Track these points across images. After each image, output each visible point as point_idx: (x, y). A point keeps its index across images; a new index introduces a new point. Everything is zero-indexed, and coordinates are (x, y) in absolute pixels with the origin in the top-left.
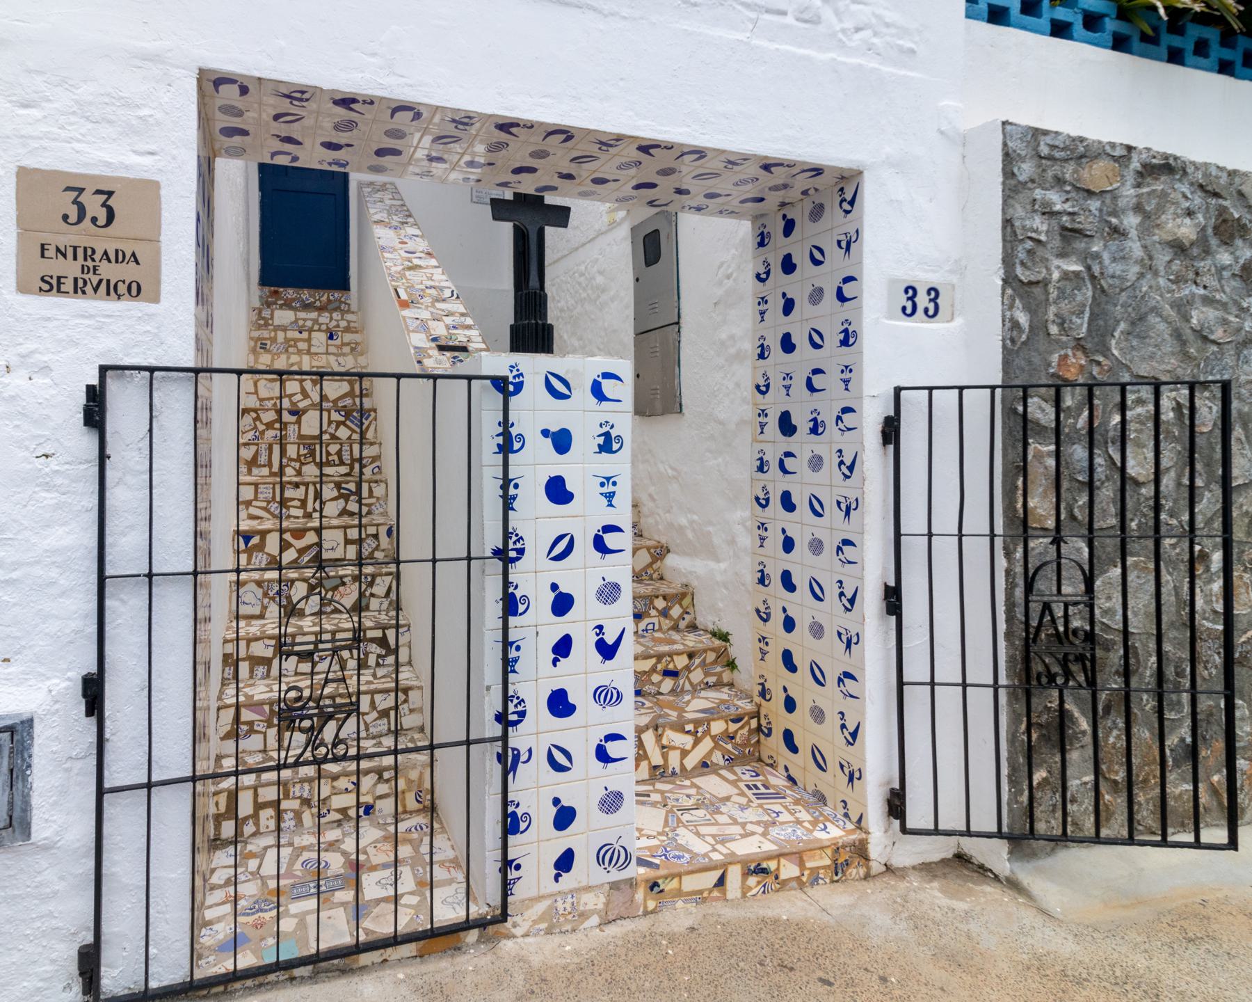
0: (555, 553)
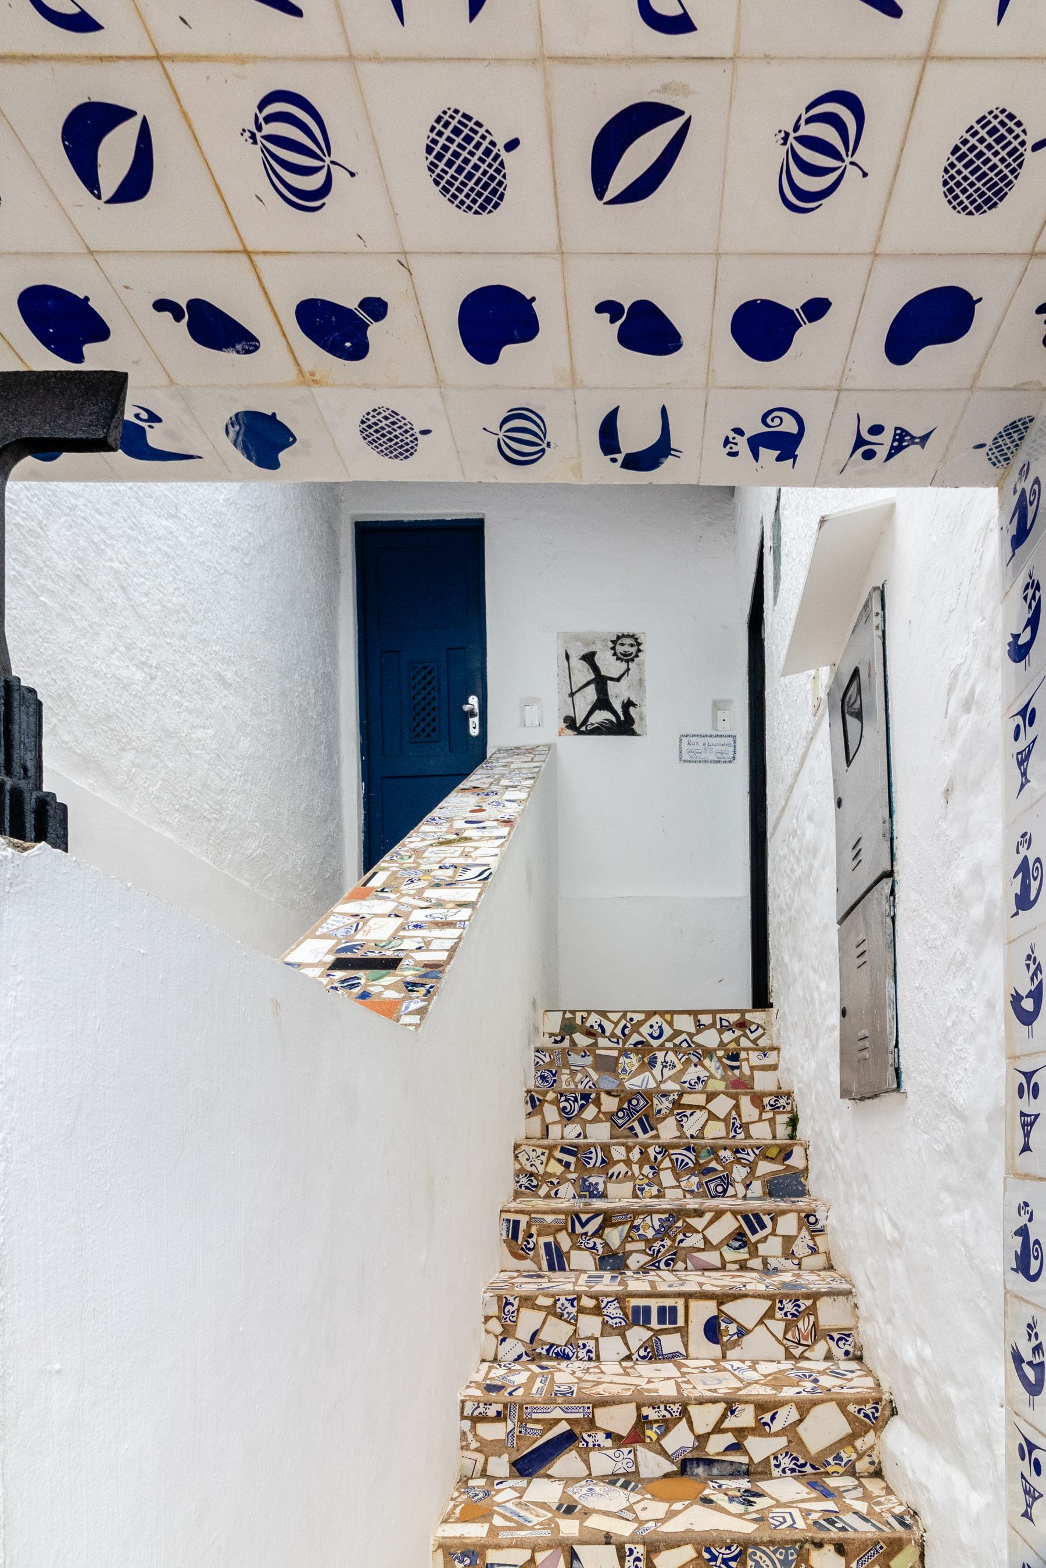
0: (663, 134)
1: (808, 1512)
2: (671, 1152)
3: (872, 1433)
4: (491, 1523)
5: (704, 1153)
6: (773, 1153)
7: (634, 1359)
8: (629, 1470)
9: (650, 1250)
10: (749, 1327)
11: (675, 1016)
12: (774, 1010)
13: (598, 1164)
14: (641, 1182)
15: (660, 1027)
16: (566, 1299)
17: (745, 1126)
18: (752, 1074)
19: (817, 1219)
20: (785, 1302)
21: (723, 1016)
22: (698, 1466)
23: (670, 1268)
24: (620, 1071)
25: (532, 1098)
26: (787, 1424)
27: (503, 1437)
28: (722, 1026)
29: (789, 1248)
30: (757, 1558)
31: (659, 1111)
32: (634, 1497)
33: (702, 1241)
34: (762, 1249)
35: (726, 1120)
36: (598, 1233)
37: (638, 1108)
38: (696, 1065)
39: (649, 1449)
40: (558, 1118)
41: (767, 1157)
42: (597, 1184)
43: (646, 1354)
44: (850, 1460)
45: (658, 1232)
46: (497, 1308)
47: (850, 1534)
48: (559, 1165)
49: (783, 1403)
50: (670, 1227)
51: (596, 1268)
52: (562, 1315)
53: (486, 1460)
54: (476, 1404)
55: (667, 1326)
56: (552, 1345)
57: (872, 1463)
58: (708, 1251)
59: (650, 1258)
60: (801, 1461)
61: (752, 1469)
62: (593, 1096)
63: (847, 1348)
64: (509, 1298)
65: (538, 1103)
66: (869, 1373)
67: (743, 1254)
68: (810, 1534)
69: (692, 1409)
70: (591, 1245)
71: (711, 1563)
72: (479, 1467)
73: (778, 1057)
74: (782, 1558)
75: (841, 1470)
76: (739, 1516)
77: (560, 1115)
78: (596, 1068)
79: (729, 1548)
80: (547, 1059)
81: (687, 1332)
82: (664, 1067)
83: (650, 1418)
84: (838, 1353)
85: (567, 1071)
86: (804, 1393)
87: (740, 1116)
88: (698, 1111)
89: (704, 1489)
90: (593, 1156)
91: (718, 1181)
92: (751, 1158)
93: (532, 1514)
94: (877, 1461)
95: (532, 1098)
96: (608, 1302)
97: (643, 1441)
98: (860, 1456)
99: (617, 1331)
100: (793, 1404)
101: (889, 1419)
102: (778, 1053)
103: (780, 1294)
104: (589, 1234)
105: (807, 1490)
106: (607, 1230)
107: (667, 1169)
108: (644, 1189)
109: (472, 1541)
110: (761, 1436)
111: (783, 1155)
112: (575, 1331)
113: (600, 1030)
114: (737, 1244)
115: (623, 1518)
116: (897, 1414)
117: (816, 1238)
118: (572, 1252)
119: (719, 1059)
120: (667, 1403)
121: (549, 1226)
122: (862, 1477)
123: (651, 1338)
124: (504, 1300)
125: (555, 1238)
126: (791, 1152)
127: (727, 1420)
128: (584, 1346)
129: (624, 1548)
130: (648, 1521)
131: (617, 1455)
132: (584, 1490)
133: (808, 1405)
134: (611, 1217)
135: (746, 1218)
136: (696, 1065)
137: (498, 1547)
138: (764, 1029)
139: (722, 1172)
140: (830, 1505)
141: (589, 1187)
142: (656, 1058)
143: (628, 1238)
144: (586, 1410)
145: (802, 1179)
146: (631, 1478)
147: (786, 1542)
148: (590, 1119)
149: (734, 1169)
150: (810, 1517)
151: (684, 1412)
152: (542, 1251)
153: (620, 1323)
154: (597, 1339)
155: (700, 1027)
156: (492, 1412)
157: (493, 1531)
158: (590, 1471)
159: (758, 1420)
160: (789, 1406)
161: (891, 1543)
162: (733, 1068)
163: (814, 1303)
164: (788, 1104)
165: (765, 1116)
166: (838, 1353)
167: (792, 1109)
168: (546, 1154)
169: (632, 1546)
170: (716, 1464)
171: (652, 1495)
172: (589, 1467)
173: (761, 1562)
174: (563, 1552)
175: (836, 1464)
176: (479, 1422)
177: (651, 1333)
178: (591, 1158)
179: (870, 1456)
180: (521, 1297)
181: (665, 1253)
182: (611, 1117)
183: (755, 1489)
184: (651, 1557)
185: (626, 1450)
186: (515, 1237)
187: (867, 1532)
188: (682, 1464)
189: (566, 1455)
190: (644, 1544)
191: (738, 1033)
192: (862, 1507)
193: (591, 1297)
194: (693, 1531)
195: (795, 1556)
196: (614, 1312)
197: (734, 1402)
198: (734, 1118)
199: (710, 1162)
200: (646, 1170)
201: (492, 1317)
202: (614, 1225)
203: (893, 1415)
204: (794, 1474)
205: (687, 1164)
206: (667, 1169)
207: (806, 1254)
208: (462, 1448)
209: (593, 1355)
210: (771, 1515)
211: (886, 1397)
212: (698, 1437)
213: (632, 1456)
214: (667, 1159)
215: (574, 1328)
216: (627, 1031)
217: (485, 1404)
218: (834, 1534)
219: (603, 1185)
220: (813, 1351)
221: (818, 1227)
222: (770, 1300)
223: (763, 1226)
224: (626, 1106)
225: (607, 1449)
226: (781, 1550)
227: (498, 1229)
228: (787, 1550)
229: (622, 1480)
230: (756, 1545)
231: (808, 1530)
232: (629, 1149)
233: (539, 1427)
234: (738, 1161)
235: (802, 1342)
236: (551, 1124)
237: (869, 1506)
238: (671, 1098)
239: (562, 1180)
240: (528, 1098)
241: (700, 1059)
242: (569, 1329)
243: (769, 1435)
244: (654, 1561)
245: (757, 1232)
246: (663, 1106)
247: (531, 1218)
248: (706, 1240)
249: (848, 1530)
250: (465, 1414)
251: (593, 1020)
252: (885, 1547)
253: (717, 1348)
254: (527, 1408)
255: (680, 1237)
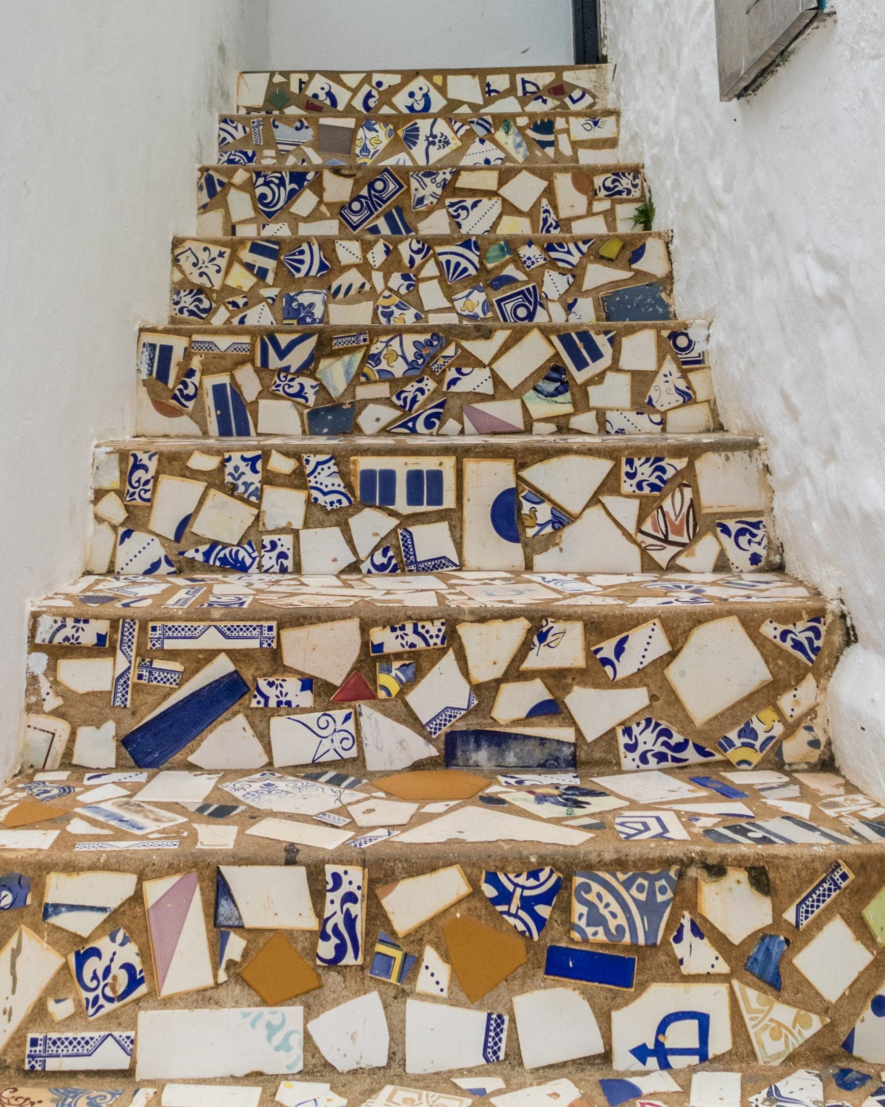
1: (694, 817)
2: (439, 249)
3: (809, 683)
4: (64, 830)
5: (493, 251)
6: (612, 249)
7: (365, 571)
8: (346, 755)
9: (398, 398)
10: (574, 507)
11: (450, 78)
12: (610, 66)
13: (313, 272)
14: (386, 303)
15: (426, 96)
16: (243, 459)
17: (564, 224)
18: (575, 153)
19: (690, 342)
20: (637, 463)
21: (528, 77)
22: (478, 746)
23: (434, 430)
24: (358, 151)
25: (210, 180)
26: (646, 662)
27: (107, 686)
28: (525, 92)
29: (643, 394)
30: (591, 897)
31: (421, 201)
32: (349, 796)
33: (490, 381)
34: (597, 396)
35: (531, 214)
36: (308, 368)
37: (385, 196)
38: (482, 141)
39: (387, 713)
40: (252, 214)
41: (602, 257)
42: (311, 305)
43: (385, 560)
44: (772, 738)
45: (412, 366)
46: (117, 474)
47: (780, 849)
48: (248, 274)
49: (638, 620)
50: (433, 357)
51: (304, 432)
52: (234, 487)
53: (73, 734)
54: (59, 619)
55: (425, 508)
56: (214, 544)
57: (814, 744)
58: (501, 399)
59: (397, 413)
60: (677, 738)
61: (582, 755)
62: (310, 176)
63: (755, 548)
64: (140, 455)
65: (219, 189)
66: (799, 583)
67: (562, 406)
68: (698, 848)
69: (465, 631)
70: (295, 389)
71: (500, 908)
72: (59, 747)
73: (618, 126)
74: (642, 897)
75: (755, 757)
76: (557, 821)
77: (255, 208)
78: (318, 147)
79: (534, 874)
80: (239, 134)
81: (461, 520)
82: (430, 143)
83: (387, 650)
84: (739, 558)
85: (272, 153)
86: (676, 604)
87: (555, 208)
88: (485, 200)
89: (489, 785)
90: (306, 257)
91: (519, 300)
92: (575, 259)
93: (147, 817)
94: (823, 740)
95: (210, 180)
96: (318, 464)
97: (373, 697)
98: (791, 730)
99: (333, 518)
100: (657, 621)
101: (841, 651)
102: (618, 121)
103: (627, 448)
104: (292, 370)
105: (691, 787)
106: (324, 363)
107: (431, 278)
108: (392, 313)
109: (20, 855)
110: (597, 686)
111: (628, 254)
112: (258, 517)
113: (328, 102)
114: (551, 387)
115: (326, 824)
116: (856, 640)
117: (692, 376)
118: (262, 403)
119: (521, 130)
120: (418, 618)
121: (222, 356)
122: (796, 771)
123: (394, 530)
124: (132, 460)
125: (233, 377)
126: (643, 248)
127: (532, 654)
128: (274, 545)
129: (323, 872)
130: (374, 828)
131: (323, 724)
132: (256, 786)
133: (685, 625)
134: (331, 339)
135: (566, 340)
136: (482, 141)
137: (71, 868)
138: (594, 97)
139: (526, 283)
140: (737, 807)
141: (298, 311)
142: (417, 129)
143: (359, 378)
144: (266, 633)
145: (663, 295)
146: (349, 769)
147: (651, 863)
148: (305, 214)
149: (546, 278)
150: (697, 824)
151: (451, 638)
152: (209, 401)
153: (339, 501)
154: (296, 533)
155: (491, 95)
156: (88, 637)
157: (66, 841)
158: (270, 756)
159: (591, 653)
160: (649, 625)
161: (863, 867)
162: (543, 145)
163: (691, 465)
164: (635, 186)
165: (598, 207)
166: (739, 558)
167: (643, 195)
168: (227, 255)
169: (340, 869)
170: (513, 744)
171: (387, 793)
172: (268, 748)
173: (601, 906)
174: (201, 880)
175: (744, 745)
176: (64, 656)
177: (395, 522)
178: (302, 262)
179: (809, 729)
180: (161, 454)
181: (424, 404)
182: (341, 210)
183: (588, 786)
184: (378, 892)
185: (339, 714)
186: (163, 375)
187: (812, 845)
188: (447, 743)
189: (226, 724)
190: (364, 864)
191: (552, 103)
192: (803, 810)
193: (287, 454)
194: (462, 842)
195: (669, 894)
196: (329, 481)
197: (545, 617)
198: (546, 211)
199: (503, 266)
200: (396, 281)
201: (108, 491)
202: (336, 354)
203: (848, 643)
204: (664, 765)
205: (465, 270)
206: (431, 278)
207: (674, 404)
208: (29, 708)
209: (289, 563)
210: (618, 820)
211: (833, 606)
212: (477, 689)
213: (350, 725)
214: (432, 262)
215: (255, 511)
216: (372, 103)
217: (77, 621)
218: (746, 847)
219: (322, 308)
220: (693, 554)
221: (694, 354)
222: (611, 458)
223: (596, 354)
224: (364, 192)
225: (304, 711)
226: (640, 880)
227: (134, 361)
228: (652, 879)
229: (331, 774)
230: (589, 868)
231: (693, 842)
232: (367, 247)
233: (176, 666)
234: (552, 264)
235: (672, 537)
236: (240, 222)
237: (814, 808)
238: (439, 179)
239: (252, 299)
240: (203, 181)
241: (489, 131)
242: (247, 514)
243: (614, 684)
244: (384, 902)
245: (587, 364)
246: (427, 192)
247: (192, 342)
248: (496, 380)
249: (774, 842)
250: (38, 640)
251: (318, 86)
252: (851, 876)
253: (514, 552)
254: (154, 629)
255: (452, 374)
